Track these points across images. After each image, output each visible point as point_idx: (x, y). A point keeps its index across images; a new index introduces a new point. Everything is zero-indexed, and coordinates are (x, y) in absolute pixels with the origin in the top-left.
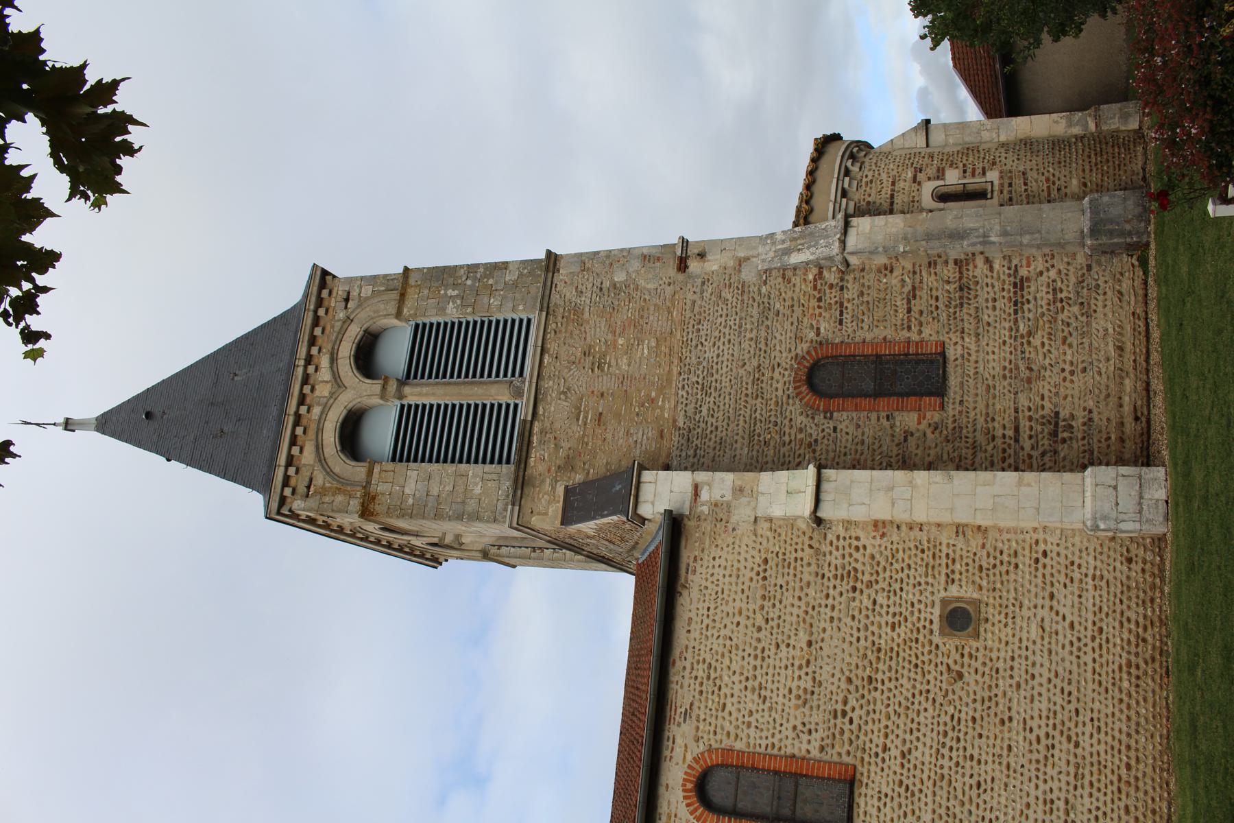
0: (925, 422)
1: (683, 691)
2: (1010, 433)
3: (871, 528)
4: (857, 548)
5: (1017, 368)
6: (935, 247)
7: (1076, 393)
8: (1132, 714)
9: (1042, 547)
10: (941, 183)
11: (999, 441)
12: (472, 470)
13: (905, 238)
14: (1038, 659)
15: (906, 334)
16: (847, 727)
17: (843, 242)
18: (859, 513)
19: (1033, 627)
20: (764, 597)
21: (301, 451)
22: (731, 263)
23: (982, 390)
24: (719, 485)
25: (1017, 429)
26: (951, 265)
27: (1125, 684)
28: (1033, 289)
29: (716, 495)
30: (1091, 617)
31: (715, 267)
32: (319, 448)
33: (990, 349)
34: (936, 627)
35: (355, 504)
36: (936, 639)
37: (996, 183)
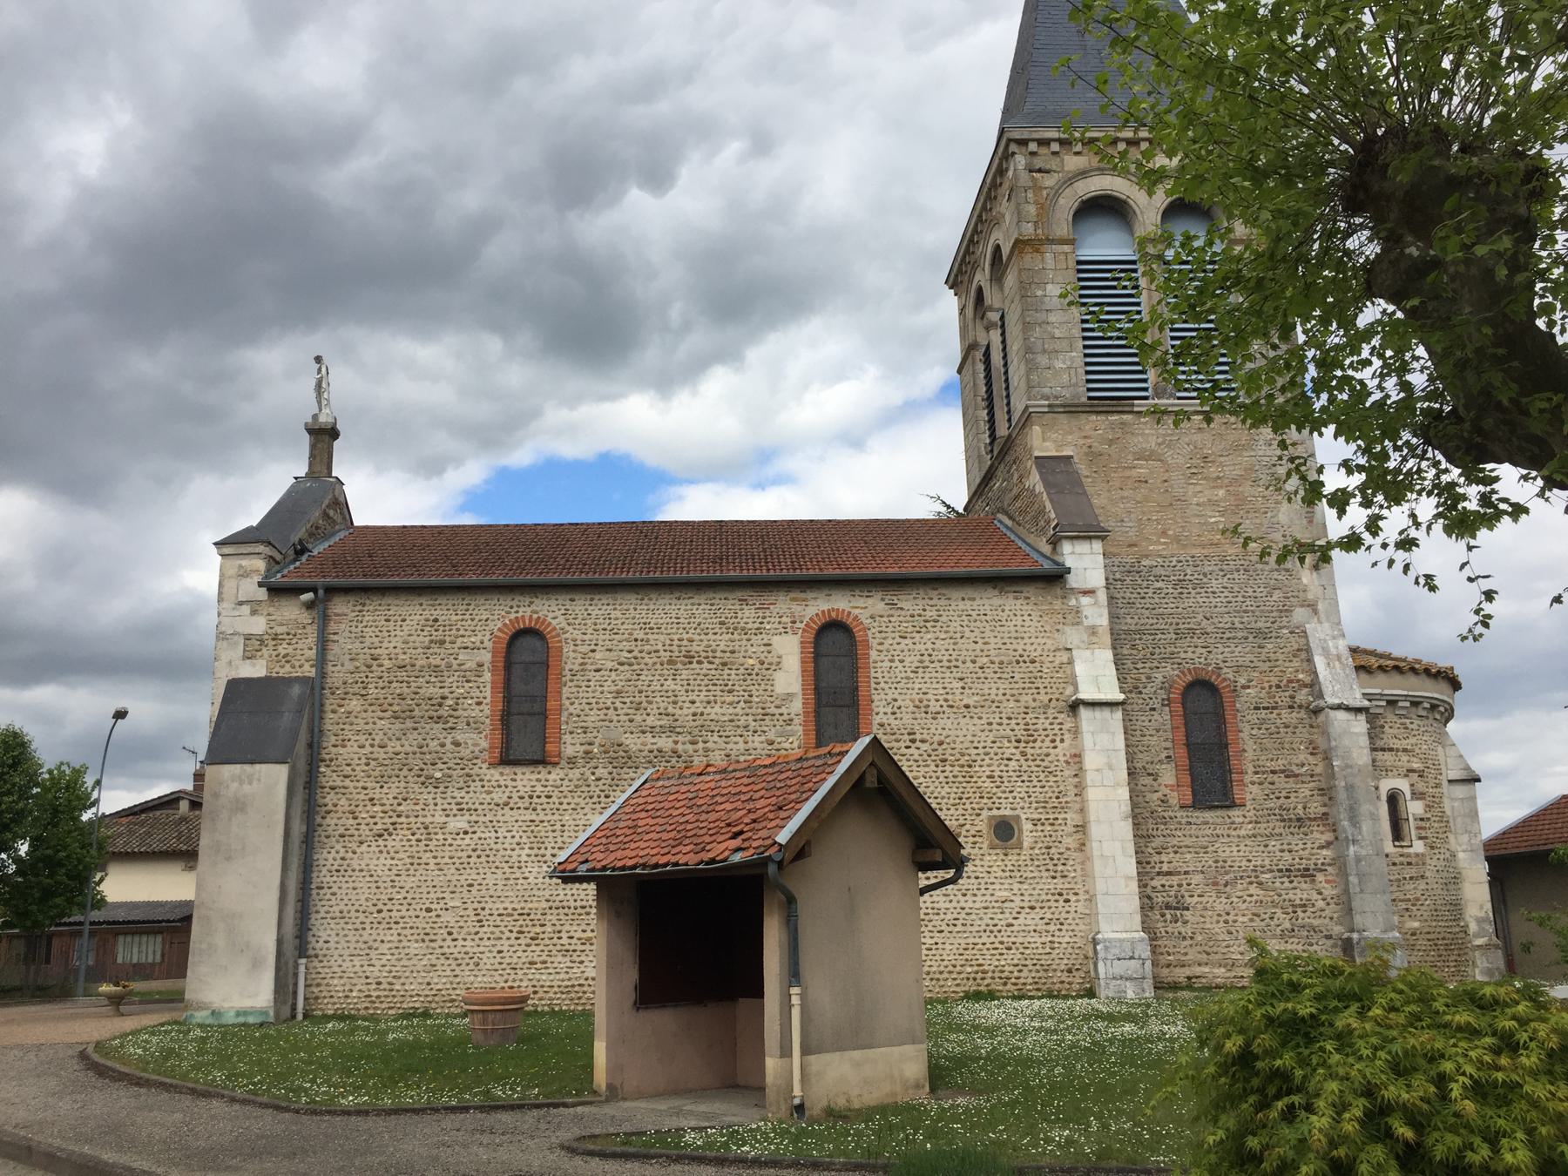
0: (1167, 791)
1: (911, 603)
2: (1165, 868)
3: (1073, 751)
4: (1053, 741)
5: (1226, 873)
6: (1342, 795)
7: (1208, 926)
8: (946, 975)
9: (1073, 898)
10: (1408, 796)
11: (1156, 858)
12: (1077, 356)
13: (1347, 766)
14: (978, 899)
15: (1251, 769)
16: (902, 744)
17: (1339, 707)
18: (1087, 740)
19: (1005, 894)
20: (1001, 663)
21: (1077, 153)
22: (1310, 596)
23: (1203, 841)
24: (1096, 613)
25: (1169, 873)
26: (1324, 810)
27: (969, 969)
28: (1304, 886)
29: (1087, 611)
30: (1020, 940)
31: (1305, 581)
32: (1083, 174)
33: (1242, 847)
34: (995, 812)
35: (1028, 230)
36: (985, 813)
37: (1411, 850)
